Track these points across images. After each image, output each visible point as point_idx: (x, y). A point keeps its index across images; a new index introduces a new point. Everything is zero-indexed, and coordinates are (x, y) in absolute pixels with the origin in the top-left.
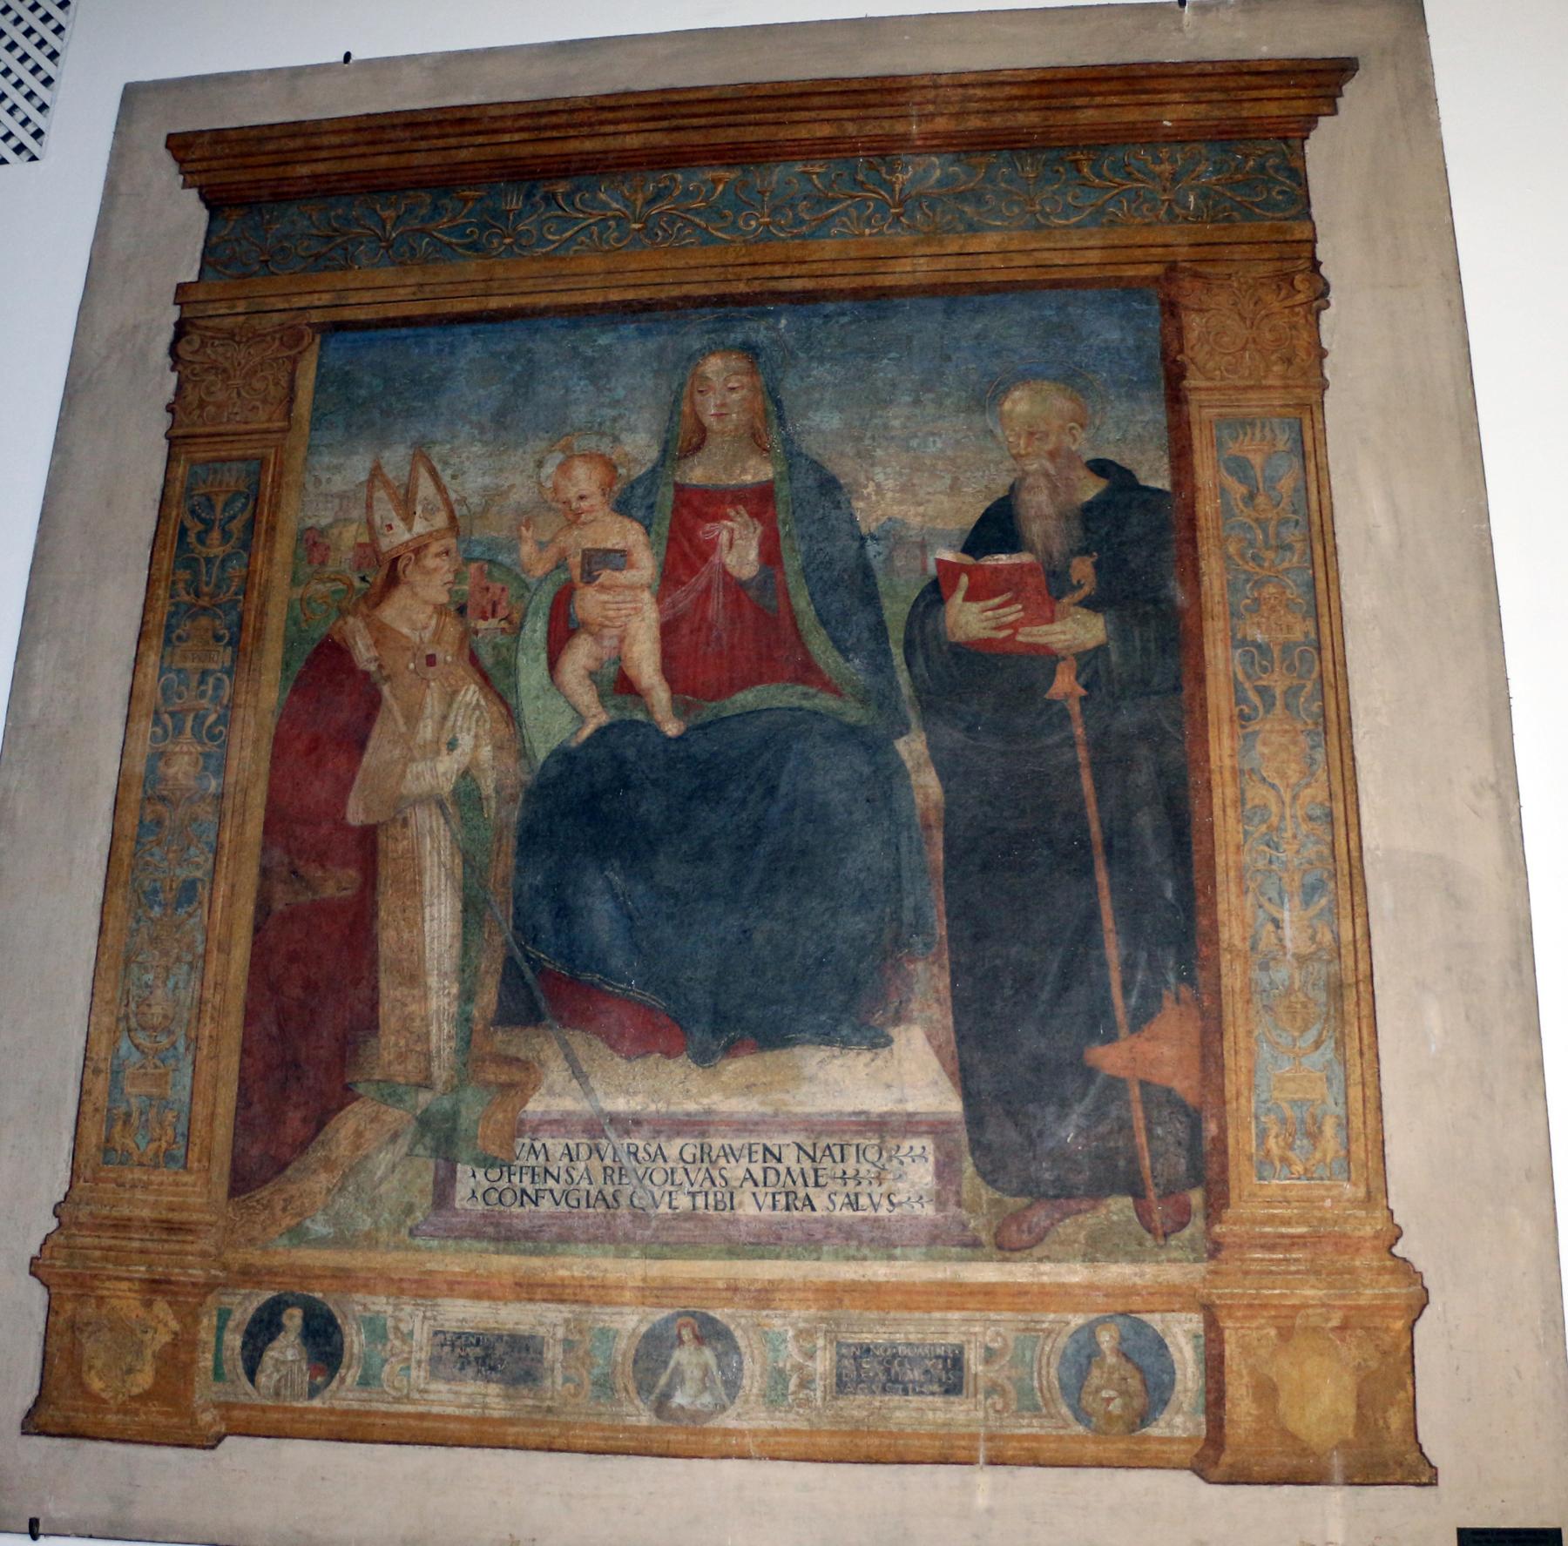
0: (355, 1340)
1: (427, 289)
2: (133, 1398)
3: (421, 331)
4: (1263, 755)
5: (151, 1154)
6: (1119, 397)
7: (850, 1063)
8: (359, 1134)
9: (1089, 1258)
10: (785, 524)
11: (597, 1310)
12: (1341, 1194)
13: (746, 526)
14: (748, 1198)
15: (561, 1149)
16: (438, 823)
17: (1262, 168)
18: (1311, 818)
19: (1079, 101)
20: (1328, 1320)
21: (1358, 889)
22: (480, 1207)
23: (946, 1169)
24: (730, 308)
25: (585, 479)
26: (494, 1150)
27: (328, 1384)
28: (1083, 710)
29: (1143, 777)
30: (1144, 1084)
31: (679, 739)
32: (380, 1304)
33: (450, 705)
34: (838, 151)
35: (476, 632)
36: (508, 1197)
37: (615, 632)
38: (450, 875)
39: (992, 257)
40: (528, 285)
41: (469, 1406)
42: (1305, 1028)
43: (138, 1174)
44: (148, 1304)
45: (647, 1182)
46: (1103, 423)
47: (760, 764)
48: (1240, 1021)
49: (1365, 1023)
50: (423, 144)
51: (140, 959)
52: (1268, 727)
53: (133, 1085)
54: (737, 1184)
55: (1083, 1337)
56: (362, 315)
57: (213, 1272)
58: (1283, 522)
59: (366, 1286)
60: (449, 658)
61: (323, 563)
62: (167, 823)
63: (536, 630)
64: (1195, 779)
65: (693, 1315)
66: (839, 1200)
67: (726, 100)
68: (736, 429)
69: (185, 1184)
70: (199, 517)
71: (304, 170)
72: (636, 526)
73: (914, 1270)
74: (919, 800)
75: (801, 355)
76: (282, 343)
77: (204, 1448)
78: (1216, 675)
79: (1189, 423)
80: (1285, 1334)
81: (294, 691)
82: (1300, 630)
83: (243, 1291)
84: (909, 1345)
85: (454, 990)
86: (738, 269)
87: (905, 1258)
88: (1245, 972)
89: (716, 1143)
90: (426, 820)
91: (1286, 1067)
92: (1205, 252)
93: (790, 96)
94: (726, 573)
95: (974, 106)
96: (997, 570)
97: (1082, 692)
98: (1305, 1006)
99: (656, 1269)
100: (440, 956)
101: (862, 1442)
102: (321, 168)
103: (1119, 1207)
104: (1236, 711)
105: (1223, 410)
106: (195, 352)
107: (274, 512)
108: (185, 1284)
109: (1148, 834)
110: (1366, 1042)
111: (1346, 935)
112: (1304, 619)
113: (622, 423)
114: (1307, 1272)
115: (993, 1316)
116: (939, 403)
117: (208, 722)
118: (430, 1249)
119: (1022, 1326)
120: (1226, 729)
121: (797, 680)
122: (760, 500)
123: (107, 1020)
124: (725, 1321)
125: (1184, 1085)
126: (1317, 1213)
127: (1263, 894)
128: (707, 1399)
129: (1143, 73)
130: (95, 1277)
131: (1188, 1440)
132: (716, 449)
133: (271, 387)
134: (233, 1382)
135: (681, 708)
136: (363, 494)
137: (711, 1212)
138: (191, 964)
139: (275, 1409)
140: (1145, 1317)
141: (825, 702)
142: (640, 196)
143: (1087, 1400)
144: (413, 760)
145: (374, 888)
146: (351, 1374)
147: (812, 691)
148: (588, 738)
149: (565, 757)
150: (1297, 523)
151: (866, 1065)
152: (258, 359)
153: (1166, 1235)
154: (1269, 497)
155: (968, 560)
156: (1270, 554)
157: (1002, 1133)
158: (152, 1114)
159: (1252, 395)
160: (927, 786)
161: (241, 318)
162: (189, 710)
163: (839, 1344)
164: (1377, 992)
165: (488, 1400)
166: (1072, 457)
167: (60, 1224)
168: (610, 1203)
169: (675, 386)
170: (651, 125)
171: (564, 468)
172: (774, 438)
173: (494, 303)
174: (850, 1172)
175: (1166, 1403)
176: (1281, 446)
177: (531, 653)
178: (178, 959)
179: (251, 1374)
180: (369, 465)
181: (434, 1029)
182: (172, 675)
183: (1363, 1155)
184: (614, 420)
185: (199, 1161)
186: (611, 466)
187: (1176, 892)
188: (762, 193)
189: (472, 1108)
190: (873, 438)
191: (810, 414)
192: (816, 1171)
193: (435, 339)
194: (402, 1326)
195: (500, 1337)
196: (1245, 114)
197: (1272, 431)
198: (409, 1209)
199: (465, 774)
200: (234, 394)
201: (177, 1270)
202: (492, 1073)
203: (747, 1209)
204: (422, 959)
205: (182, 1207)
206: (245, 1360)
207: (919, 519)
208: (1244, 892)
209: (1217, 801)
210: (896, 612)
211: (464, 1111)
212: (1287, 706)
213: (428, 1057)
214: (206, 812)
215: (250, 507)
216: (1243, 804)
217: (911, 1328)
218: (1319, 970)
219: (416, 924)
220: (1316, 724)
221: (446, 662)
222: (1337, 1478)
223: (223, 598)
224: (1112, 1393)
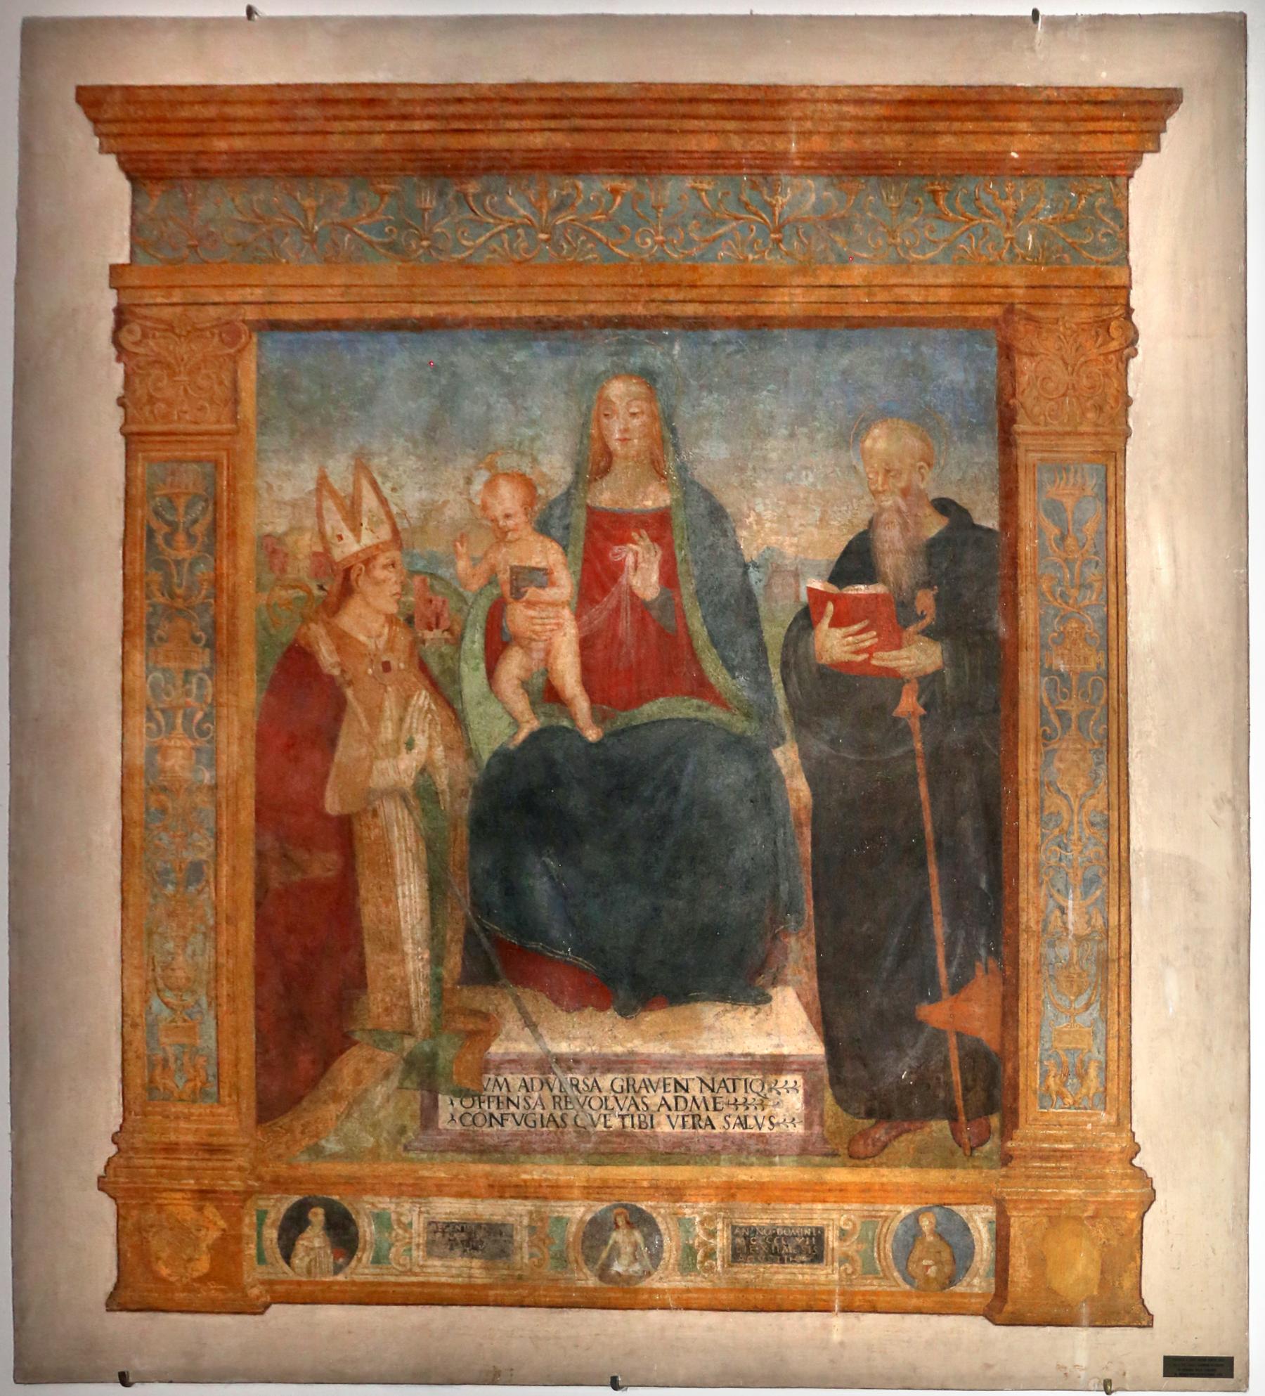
0: (367, 1229)
1: (354, 290)
2: (194, 1280)
3: (350, 335)
4: (1059, 770)
5: (188, 1091)
6: (960, 438)
7: (739, 1015)
8: (358, 1072)
9: (916, 1164)
10: (681, 549)
11: (553, 1203)
12: (1099, 1120)
13: (649, 551)
14: (663, 1119)
15: (519, 1083)
16: (403, 814)
17: (1091, 208)
18: (1093, 824)
19: (941, 126)
20: (1084, 1211)
21: (1125, 884)
22: (458, 1127)
23: (810, 1099)
24: (630, 330)
25: (508, 498)
26: (467, 1083)
27: (348, 1263)
28: (922, 728)
29: (967, 787)
30: (959, 1035)
31: (599, 744)
32: (386, 1203)
33: (405, 709)
34: (725, 167)
35: (424, 642)
36: (480, 1120)
37: (541, 645)
38: (416, 859)
39: (858, 291)
40: (444, 294)
41: (459, 1276)
42: (1080, 993)
43: (180, 1108)
44: (200, 1209)
45: (586, 1107)
46: (946, 464)
47: (665, 767)
48: (1032, 987)
49: (1123, 989)
50: (337, 126)
51: (160, 930)
52: (1064, 746)
53: (167, 1036)
54: (654, 1108)
55: (910, 1222)
56: (294, 315)
57: (250, 1183)
58: (1086, 563)
59: (373, 1190)
60: (402, 666)
61: (283, 570)
62: (170, 810)
63: (475, 642)
64: (1007, 789)
65: (625, 1207)
66: (732, 1120)
67: (621, 101)
68: (638, 455)
69: (220, 1115)
70: (162, 517)
71: (221, 144)
72: (555, 546)
73: (786, 1172)
74: (792, 803)
75: (693, 382)
76: (222, 340)
77: (255, 1314)
78: (1026, 699)
79: (1016, 466)
80: (1054, 1221)
81: (270, 692)
82: (1094, 661)
83: (275, 1196)
84: (785, 1227)
85: (426, 956)
86: (636, 291)
87: (782, 1164)
88: (1037, 949)
89: (639, 1077)
90: (392, 811)
91: (1063, 1023)
92: (1038, 295)
93: (682, 101)
94: (633, 595)
95: (848, 125)
96: (857, 599)
97: (922, 711)
98: (1079, 975)
99: (598, 1172)
100: (413, 927)
101: (751, 1297)
102: (239, 143)
103: (939, 1127)
104: (1040, 732)
105: (1046, 455)
106: (136, 344)
107: (232, 519)
108: (227, 1193)
109: (970, 833)
110: (1123, 1005)
111: (1113, 921)
112: (1098, 651)
113: (538, 444)
114: (1072, 1176)
115: (846, 1207)
116: (811, 439)
117: (196, 721)
118: (421, 1161)
119: (866, 1213)
120: (1032, 746)
121: (692, 694)
122: (659, 524)
123: (137, 982)
124: (649, 1210)
125: (987, 1035)
126: (1081, 1134)
127: (1053, 886)
128: (637, 1267)
129: (997, 98)
130: (154, 1189)
131: (983, 1295)
132: (622, 474)
133: (216, 387)
134: (272, 1264)
135: (599, 718)
136: (314, 502)
137: (637, 1130)
138: (204, 934)
139: (310, 1283)
140: (955, 1208)
141: (715, 713)
142: (545, 203)
143: (912, 1267)
144: (377, 758)
145: (353, 869)
146: (366, 1256)
147: (705, 704)
148: (524, 741)
149: (504, 757)
150: (1097, 564)
151: (752, 1018)
152: (199, 356)
153: (972, 1149)
154: (1077, 540)
155: (833, 589)
156: (1074, 592)
157: (850, 1071)
158: (186, 1059)
159: (1068, 440)
160: (799, 789)
161: (179, 309)
162: (180, 707)
163: (734, 1228)
164: (1133, 966)
165: (473, 1271)
166: (921, 494)
167: (119, 1150)
168: (560, 1124)
169: (584, 407)
170: (552, 124)
171: (491, 485)
172: (670, 466)
173: (418, 311)
174: (741, 1100)
175: (967, 1270)
176: (1089, 491)
177: (473, 663)
178: (194, 930)
179: (287, 1258)
180: (315, 474)
181: (412, 987)
182: (158, 675)
183: (1115, 1091)
184: (533, 440)
185: (230, 1096)
186: (529, 485)
187: (990, 883)
188: (656, 208)
189: (447, 1053)
190: (754, 469)
191: (701, 443)
192: (715, 1099)
193: (367, 345)
194: (403, 1219)
195: (479, 1226)
196: (1081, 148)
197: (1083, 476)
198: (403, 1130)
199: (423, 771)
200: (181, 392)
201: (221, 1182)
202: (460, 1023)
203: (664, 1128)
204: (398, 931)
205: (219, 1133)
206: (282, 1249)
207: (793, 549)
208: (1039, 884)
209: (1022, 808)
210: (774, 634)
211: (440, 1053)
212: (1079, 728)
213: (409, 1010)
214: (202, 799)
215: (211, 508)
216: (1042, 812)
217: (786, 1216)
218: (1092, 948)
219: (390, 900)
220: (1101, 744)
221: (399, 669)
222: (1085, 1322)
223: (197, 600)
224: (930, 1262)
